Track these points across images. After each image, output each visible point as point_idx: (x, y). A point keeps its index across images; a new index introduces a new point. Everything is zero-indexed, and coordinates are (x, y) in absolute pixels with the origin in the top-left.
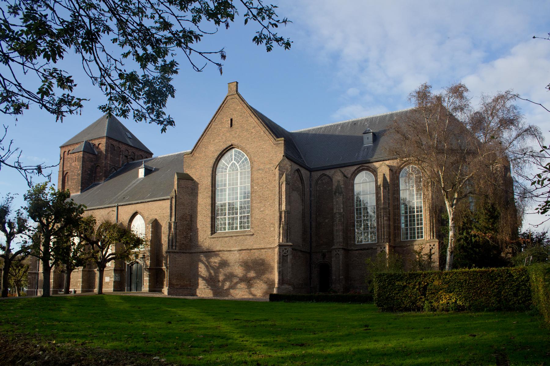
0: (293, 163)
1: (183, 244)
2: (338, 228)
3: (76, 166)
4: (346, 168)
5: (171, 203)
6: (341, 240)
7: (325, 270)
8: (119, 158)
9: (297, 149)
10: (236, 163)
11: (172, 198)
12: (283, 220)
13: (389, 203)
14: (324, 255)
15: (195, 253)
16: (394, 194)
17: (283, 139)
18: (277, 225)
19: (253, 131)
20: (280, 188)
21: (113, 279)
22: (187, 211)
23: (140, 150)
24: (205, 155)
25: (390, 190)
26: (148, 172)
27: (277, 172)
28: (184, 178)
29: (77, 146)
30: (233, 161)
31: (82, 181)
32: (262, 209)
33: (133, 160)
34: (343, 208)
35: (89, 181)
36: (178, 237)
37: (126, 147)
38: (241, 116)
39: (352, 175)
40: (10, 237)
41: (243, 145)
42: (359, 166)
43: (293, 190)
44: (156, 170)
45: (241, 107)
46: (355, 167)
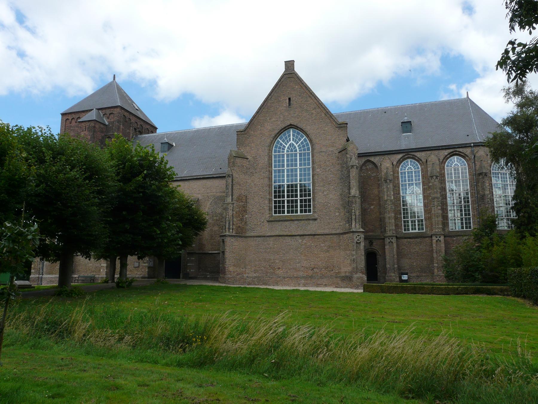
1: (239, 226)
8: (130, 130)
10: (295, 144)
15: (251, 237)
19: (313, 111)
22: (243, 192)
30: (292, 141)
32: (325, 193)
36: (235, 220)
37: (136, 119)
38: (300, 96)
39: (397, 163)
42: (404, 154)
46: (400, 156)
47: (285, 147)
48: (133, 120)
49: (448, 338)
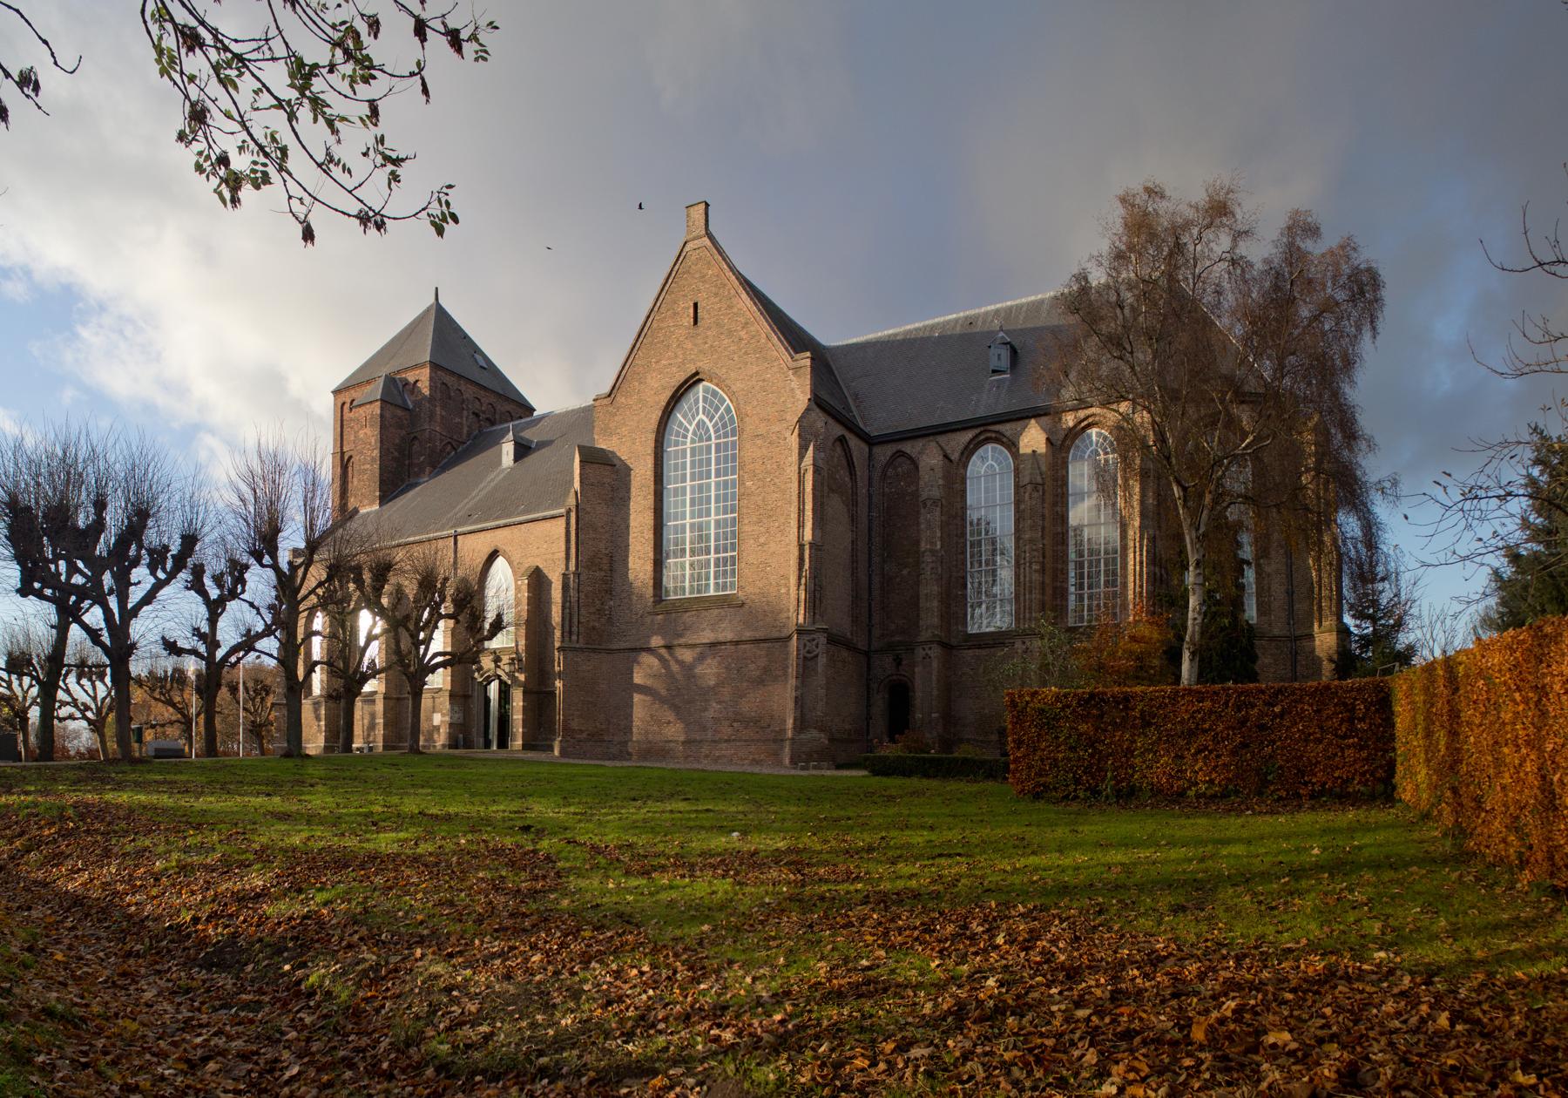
0: (831, 421)
2: (930, 589)
3: (367, 439)
4: (950, 436)
5: (568, 524)
6: (936, 621)
7: (900, 696)
9: (837, 382)
11: (569, 512)
12: (807, 566)
13: (1043, 528)
14: (898, 661)
16: (1055, 504)
17: (808, 354)
18: (793, 580)
19: (742, 333)
20: (801, 482)
21: (447, 719)
22: (602, 546)
23: (507, 399)
24: (640, 400)
25: (1044, 494)
26: (523, 450)
27: (793, 440)
28: (594, 459)
29: (369, 388)
30: (701, 416)
31: (381, 475)
32: (762, 540)
33: (493, 423)
34: (942, 539)
35: (396, 478)
36: (583, 611)
37: (475, 389)
38: (716, 294)
40: (215, 609)
41: (722, 372)
42: (977, 431)
43: (831, 490)
44: (542, 445)
45: (716, 270)
46: (969, 435)
47: (687, 430)
48: (469, 392)
49: (418, 902)
